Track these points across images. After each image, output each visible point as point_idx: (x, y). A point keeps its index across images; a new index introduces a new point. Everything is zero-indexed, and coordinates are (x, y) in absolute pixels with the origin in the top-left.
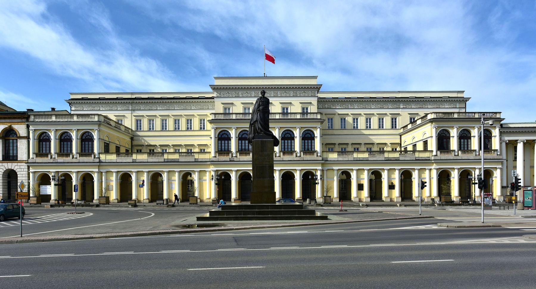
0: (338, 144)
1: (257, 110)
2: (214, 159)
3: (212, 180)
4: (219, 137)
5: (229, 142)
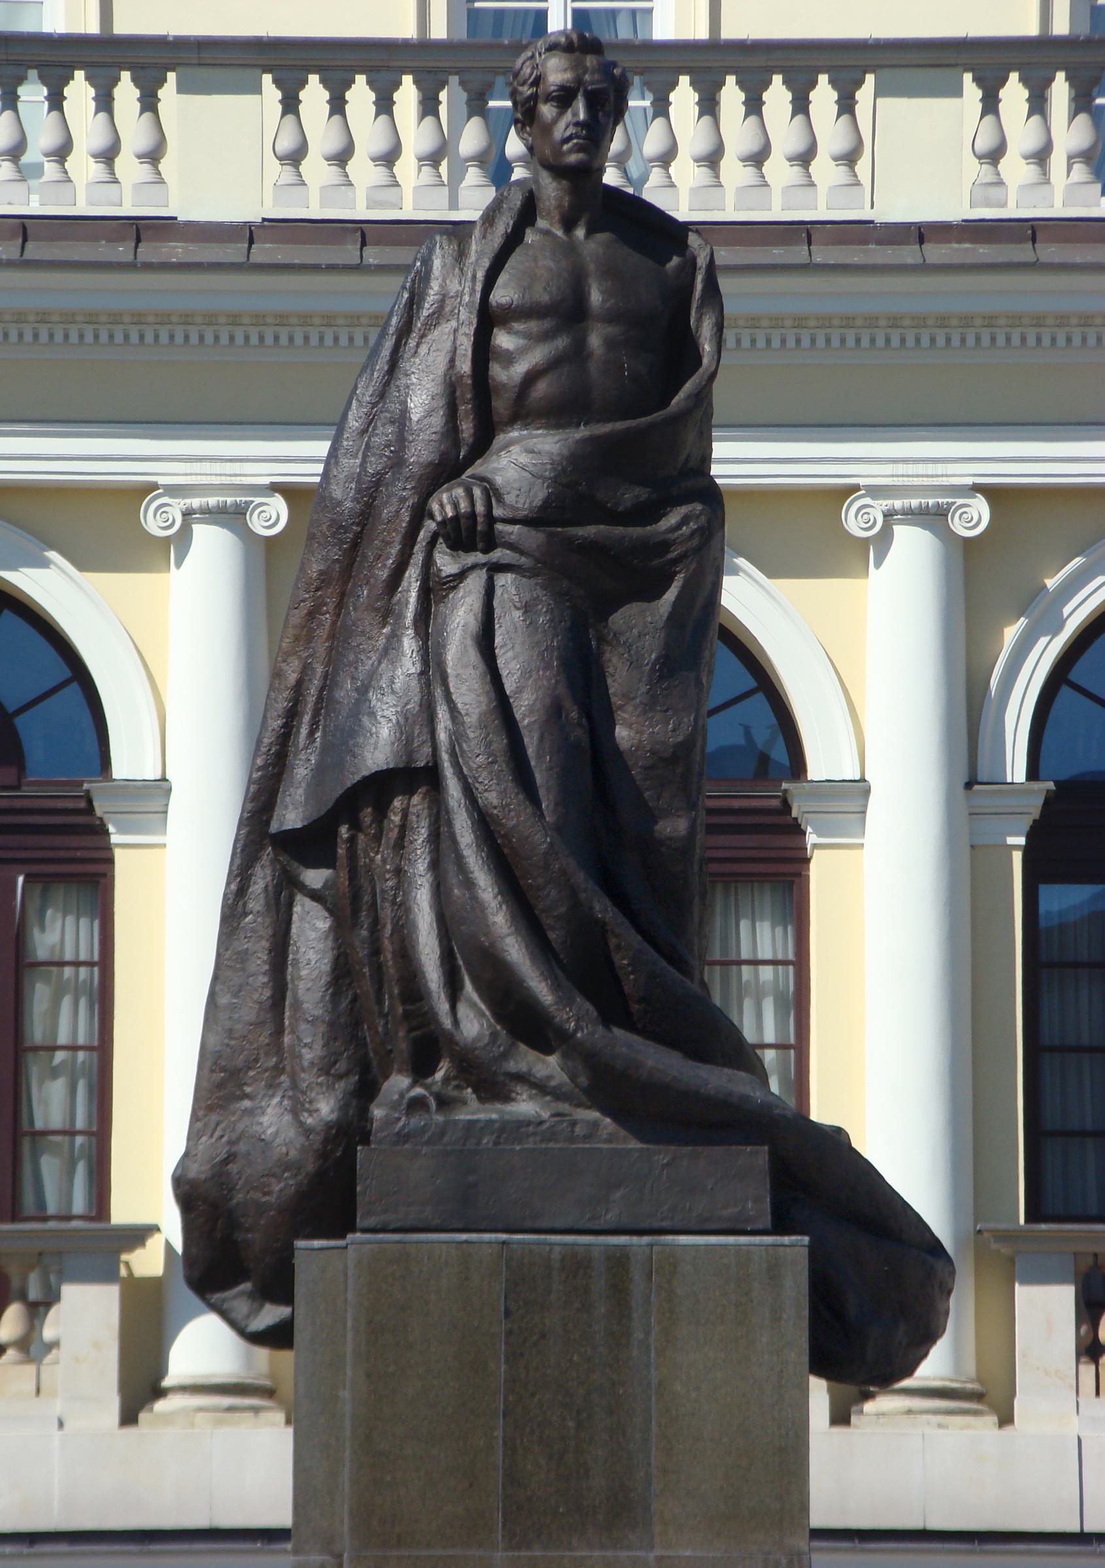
1: (420, 513)
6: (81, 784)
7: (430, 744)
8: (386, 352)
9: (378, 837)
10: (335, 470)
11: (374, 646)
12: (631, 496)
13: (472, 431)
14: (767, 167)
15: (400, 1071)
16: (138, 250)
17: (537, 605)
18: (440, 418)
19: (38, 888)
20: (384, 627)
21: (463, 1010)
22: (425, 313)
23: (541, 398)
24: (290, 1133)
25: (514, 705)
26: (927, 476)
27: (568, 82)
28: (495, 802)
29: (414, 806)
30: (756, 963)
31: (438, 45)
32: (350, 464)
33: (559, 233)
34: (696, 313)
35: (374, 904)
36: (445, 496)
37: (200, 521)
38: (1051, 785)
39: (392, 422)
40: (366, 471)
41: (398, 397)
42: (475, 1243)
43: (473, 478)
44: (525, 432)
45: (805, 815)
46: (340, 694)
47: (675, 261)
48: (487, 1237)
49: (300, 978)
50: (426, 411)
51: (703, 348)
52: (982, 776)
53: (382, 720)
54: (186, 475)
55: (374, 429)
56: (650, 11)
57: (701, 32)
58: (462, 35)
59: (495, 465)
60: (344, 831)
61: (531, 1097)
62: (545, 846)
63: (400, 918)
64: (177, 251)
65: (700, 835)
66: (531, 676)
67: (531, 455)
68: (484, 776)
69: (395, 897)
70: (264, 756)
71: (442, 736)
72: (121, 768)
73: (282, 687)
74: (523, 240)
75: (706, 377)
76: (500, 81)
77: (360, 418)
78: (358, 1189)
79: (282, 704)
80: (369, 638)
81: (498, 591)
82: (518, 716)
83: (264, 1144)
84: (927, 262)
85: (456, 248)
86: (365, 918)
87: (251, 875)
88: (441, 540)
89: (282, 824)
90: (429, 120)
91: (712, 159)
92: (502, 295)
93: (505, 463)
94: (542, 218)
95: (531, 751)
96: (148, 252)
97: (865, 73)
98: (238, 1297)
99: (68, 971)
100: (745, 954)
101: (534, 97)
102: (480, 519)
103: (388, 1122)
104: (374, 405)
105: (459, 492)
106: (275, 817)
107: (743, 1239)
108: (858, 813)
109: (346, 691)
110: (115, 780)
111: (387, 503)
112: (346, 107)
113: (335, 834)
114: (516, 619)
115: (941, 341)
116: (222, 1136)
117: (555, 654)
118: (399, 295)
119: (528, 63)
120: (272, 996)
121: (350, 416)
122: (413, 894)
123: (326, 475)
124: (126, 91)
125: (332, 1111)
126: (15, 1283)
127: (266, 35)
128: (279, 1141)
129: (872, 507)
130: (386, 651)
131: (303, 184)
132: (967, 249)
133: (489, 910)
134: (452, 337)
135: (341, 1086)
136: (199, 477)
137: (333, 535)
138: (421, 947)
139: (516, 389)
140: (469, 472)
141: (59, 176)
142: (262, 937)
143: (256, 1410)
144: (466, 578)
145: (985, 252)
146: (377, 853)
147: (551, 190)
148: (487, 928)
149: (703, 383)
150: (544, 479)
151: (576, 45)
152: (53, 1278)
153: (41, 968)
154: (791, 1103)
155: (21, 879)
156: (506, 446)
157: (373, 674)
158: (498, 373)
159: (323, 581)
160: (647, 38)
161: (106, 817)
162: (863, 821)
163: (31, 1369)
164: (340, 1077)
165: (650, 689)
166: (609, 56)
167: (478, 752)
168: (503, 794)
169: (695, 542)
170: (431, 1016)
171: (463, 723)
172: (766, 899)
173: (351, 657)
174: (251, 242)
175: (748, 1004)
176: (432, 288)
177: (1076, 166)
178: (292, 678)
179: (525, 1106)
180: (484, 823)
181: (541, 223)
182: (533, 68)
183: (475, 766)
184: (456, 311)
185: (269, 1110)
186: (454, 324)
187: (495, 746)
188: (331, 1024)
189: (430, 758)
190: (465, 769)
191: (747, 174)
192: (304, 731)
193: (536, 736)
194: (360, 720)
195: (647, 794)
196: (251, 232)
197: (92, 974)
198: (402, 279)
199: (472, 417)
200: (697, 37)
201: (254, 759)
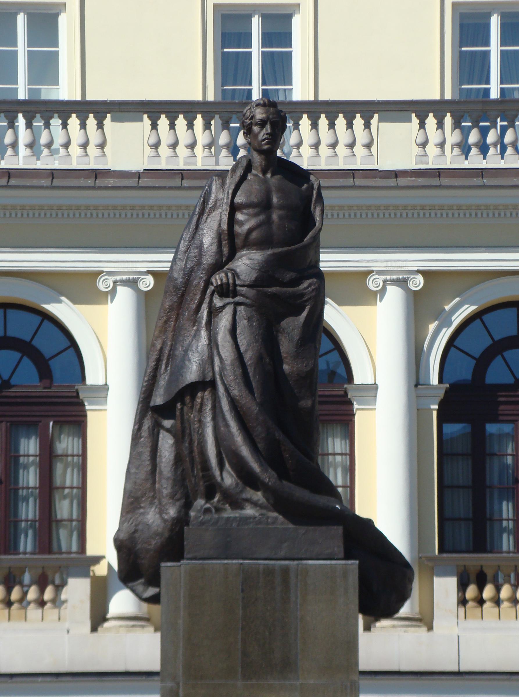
1: (208, 283)
6: (74, 386)
7: (212, 372)
8: (194, 221)
9: (192, 408)
10: (175, 267)
11: (190, 334)
12: (289, 276)
13: (227, 251)
14: (337, 149)
15: (201, 498)
16: (96, 182)
17: (253, 318)
18: (215, 247)
19: (58, 427)
20: (194, 327)
21: (225, 474)
22: (210, 206)
23: (254, 239)
24: (159, 522)
25: (245, 356)
26: (400, 267)
27: (264, 118)
28: (237, 394)
29: (206, 396)
30: (334, 454)
31: (210, 103)
32: (181, 264)
33: (261, 175)
34: (314, 206)
35: (190, 434)
36: (217, 277)
37: (120, 285)
38: (448, 386)
39: (197, 248)
40: (187, 267)
41: (199, 238)
42: (230, 564)
43: (228, 269)
44: (248, 252)
45: (354, 398)
46: (177, 353)
47: (305, 186)
48: (235, 561)
49: (162, 462)
50: (210, 244)
51: (317, 219)
52: (421, 382)
53: (193, 362)
54: (114, 267)
55: (190, 251)
56: (291, 89)
57: (311, 98)
58: (220, 99)
59: (237, 264)
60: (179, 406)
61: (251, 508)
62: (256, 411)
63: (200, 439)
64: (111, 182)
65: (318, 407)
66: (251, 346)
67: (250, 260)
68: (233, 384)
69: (199, 431)
70: (148, 377)
71: (217, 369)
72: (90, 380)
73: (155, 350)
74: (247, 178)
75: (317, 230)
76: (234, 116)
77: (184, 246)
78: (185, 543)
79: (154, 356)
80: (188, 331)
81: (238, 313)
82: (246, 360)
83: (149, 526)
84: (399, 185)
85: (221, 181)
86: (187, 438)
87: (143, 423)
88: (216, 293)
89: (154, 403)
90: (207, 131)
91: (316, 146)
92: (239, 199)
93: (240, 263)
94: (254, 170)
95: (251, 374)
96: (100, 182)
97: (374, 113)
98: (139, 584)
99: (70, 459)
100: (330, 451)
101: (251, 124)
102: (231, 285)
103: (196, 517)
104: (190, 241)
105: (223, 275)
106: (152, 400)
107: (333, 562)
108: (373, 396)
109: (179, 351)
110: (87, 385)
111: (195, 279)
112: (194, 127)
113: (175, 406)
114: (245, 324)
115: (404, 215)
116: (132, 523)
117: (260, 337)
118: (199, 200)
119: (248, 111)
120: (151, 469)
121: (180, 246)
122: (206, 430)
123: (171, 267)
124: (91, 121)
125: (175, 513)
126: (50, 578)
127: (145, 100)
128: (154, 525)
129: (378, 279)
130: (195, 336)
131: (159, 156)
132: (414, 180)
133: (235, 436)
134: (220, 215)
135: (178, 504)
136: (119, 268)
137: (174, 291)
138: (208, 450)
139: (245, 235)
140: (227, 267)
141: (66, 154)
142: (147, 447)
143: (143, 626)
144: (226, 308)
145: (421, 181)
146: (192, 414)
147: (257, 159)
148: (234, 442)
149: (317, 233)
150: (256, 270)
151: (267, 104)
152: (65, 576)
153: (60, 457)
154: (349, 507)
155: (51, 423)
156: (241, 257)
157: (190, 345)
158: (238, 229)
159: (170, 309)
160: (290, 100)
161: (84, 399)
162: (376, 399)
163: (56, 611)
164: (178, 500)
165: (297, 350)
166: (279, 107)
167: (231, 375)
168: (240, 391)
169: (314, 294)
170: (213, 477)
171: (225, 364)
172: (338, 429)
173: (181, 338)
174: (139, 178)
175: (331, 471)
176: (212, 197)
177: (455, 149)
178: (159, 346)
179: (249, 511)
180: (233, 403)
181: (254, 172)
182: (251, 113)
183: (229, 380)
184: (221, 205)
185: (150, 513)
186: (220, 210)
187: (237, 372)
188: (174, 480)
189: (212, 377)
190: (225, 382)
191: (330, 151)
192: (163, 367)
193: (253, 368)
194: (185, 363)
195: (296, 391)
196: (139, 174)
197: (79, 460)
198: (201, 192)
199: (227, 246)
200: (310, 100)
201: (144, 377)
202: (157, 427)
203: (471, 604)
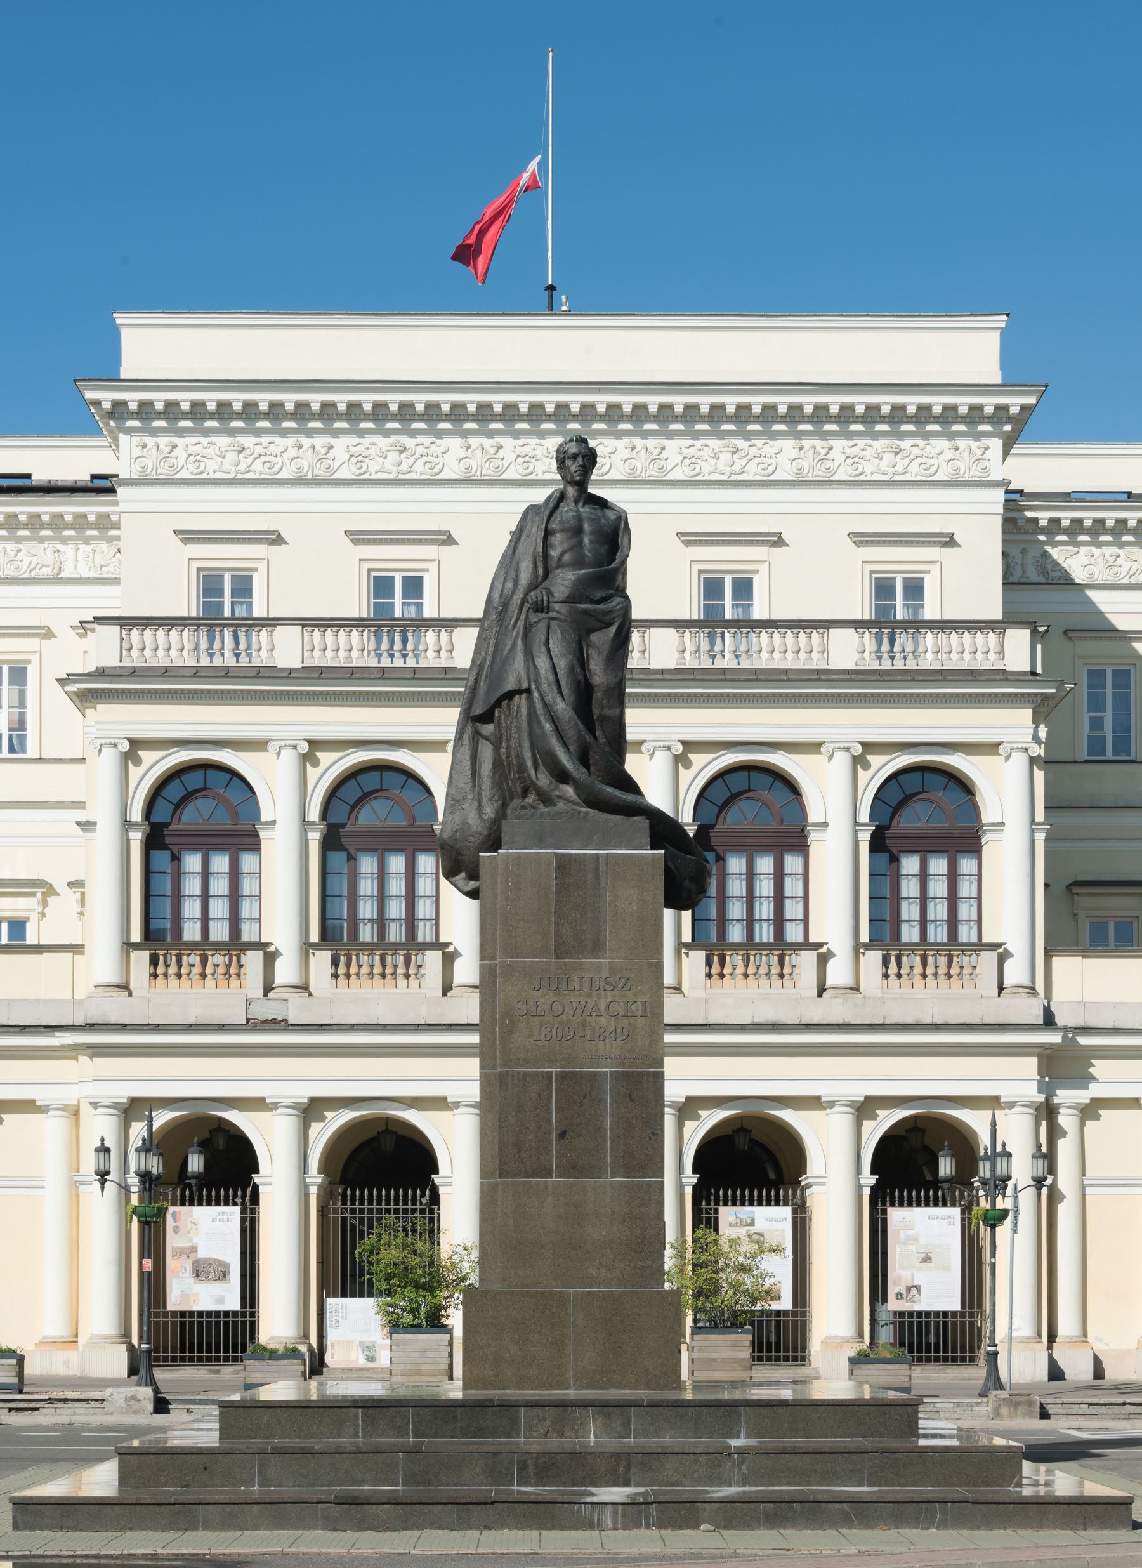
0: (1069, 887)
1: (524, 600)
2: (116, 1008)
3: (103, 1182)
4: (155, 818)
5: (248, 861)
12: (599, 594)
92: (553, 525)
147: (571, 491)
202: (477, 734)
203: (715, 977)
